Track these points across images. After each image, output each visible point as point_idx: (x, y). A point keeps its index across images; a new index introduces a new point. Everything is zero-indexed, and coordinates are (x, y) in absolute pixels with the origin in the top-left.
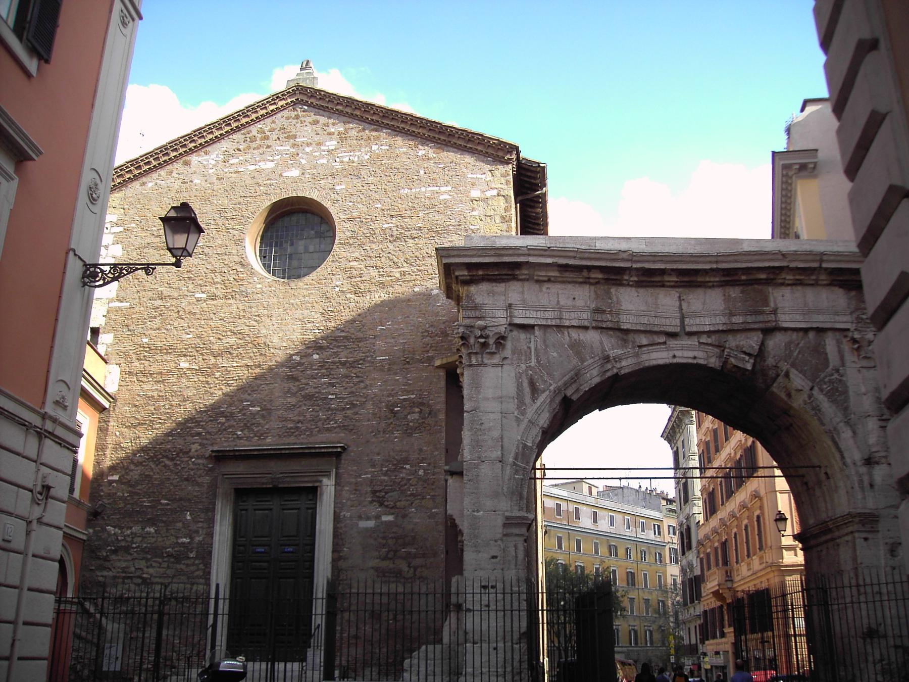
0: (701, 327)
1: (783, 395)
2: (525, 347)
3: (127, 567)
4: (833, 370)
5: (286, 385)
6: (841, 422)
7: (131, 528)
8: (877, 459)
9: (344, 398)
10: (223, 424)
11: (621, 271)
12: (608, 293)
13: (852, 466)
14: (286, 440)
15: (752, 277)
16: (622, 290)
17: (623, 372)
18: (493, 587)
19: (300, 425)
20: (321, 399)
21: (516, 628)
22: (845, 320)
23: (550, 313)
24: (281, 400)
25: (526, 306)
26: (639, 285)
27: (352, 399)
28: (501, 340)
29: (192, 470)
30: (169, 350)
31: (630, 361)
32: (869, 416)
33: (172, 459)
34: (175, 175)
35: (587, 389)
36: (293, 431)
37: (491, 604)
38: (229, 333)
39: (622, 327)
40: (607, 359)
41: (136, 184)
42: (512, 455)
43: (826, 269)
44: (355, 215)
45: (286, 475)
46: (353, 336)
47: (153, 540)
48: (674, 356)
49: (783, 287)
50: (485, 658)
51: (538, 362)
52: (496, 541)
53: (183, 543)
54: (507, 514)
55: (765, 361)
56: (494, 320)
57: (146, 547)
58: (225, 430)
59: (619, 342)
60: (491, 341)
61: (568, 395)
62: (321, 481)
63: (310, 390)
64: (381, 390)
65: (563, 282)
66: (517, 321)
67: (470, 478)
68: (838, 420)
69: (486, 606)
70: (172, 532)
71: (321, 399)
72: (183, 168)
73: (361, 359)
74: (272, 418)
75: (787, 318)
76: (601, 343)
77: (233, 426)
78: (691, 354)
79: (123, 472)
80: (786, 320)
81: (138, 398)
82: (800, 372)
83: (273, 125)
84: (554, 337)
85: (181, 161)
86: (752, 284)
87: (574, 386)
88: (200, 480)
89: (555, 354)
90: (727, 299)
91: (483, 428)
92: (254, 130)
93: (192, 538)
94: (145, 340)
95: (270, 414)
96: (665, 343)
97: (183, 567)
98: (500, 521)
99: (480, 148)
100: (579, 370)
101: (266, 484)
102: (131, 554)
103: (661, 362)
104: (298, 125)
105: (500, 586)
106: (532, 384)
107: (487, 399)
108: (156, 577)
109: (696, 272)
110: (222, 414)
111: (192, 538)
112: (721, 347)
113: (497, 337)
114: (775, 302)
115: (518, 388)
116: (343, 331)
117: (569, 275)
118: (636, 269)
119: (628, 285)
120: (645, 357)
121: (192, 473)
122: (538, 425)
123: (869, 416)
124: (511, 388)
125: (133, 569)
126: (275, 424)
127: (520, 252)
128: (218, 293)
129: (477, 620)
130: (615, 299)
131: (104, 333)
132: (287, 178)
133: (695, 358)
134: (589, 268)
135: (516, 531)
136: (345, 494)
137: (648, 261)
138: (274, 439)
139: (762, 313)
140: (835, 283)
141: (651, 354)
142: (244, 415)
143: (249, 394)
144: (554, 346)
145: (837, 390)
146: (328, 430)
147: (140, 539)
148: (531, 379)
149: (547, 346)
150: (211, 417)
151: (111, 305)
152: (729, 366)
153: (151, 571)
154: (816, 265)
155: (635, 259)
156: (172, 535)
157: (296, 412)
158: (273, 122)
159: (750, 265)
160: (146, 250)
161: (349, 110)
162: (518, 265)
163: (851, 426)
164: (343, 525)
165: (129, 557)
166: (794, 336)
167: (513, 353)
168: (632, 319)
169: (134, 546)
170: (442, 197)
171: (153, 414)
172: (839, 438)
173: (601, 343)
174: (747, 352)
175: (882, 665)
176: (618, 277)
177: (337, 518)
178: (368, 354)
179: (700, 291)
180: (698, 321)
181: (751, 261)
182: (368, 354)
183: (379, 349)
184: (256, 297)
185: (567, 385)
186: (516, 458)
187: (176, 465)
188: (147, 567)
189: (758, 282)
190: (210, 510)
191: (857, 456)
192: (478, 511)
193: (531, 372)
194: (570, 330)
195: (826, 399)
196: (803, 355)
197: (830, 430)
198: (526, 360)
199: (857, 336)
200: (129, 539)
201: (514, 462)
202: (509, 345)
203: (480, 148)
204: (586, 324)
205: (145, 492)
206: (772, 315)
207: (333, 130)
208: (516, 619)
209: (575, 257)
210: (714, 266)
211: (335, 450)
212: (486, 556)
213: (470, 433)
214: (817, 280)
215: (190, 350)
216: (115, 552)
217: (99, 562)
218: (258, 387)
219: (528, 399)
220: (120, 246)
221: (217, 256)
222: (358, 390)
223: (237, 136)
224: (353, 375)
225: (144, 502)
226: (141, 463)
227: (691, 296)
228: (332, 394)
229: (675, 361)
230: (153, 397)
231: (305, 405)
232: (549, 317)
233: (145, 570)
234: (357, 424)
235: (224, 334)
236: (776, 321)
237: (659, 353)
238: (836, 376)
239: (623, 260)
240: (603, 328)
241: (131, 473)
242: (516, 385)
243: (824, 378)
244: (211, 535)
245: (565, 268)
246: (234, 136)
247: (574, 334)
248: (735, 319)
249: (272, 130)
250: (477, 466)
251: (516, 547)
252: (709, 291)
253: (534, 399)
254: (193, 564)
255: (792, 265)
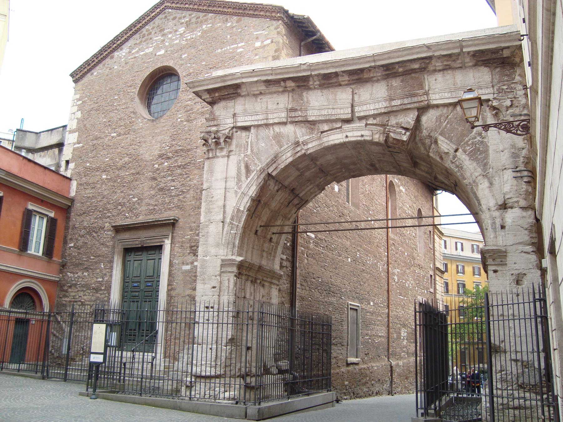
0: (368, 112)
1: (438, 159)
2: (245, 142)
3: (75, 296)
4: (476, 134)
5: (151, 183)
6: (480, 175)
7: (77, 273)
8: (510, 205)
9: (178, 188)
10: (120, 210)
11: (305, 79)
12: (301, 96)
13: (487, 211)
14: (149, 217)
15: (407, 68)
16: (311, 93)
17: (309, 152)
18: (212, 308)
19: (156, 207)
20: (167, 190)
21: (224, 336)
22: (487, 92)
23: (260, 116)
24: (148, 193)
25: (246, 113)
26: (322, 86)
27: (183, 188)
28: (228, 138)
29: (105, 238)
30: (98, 169)
31: (314, 144)
32: (505, 169)
33: (96, 233)
34: (106, 65)
35: (283, 167)
36: (152, 211)
37: (210, 319)
38: (125, 155)
39: (309, 120)
40: (297, 144)
41: (89, 75)
42: (230, 217)
43: (468, 53)
44: (191, 71)
45: (147, 239)
46: (185, 149)
47: (86, 280)
48: (347, 136)
49: (436, 73)
50: (204, 355)
51: (252, 151)
52: (216, 276)
53: (99, 281)
54: (223, 258)
55: (422, 133)
56: (225, 126)
57: (84, 284)
58: (121, 213)
59: (308, 131)
60: (222, 140)
61: (270, 172)
62: (164, 242)
63: (162, 185)
64: (198, 181)
65: (271, 93)
66: (239, 124)
67: (203, 234)
68: (477, 174)
69: (207, 320)
70: (95, 275)
71: (167, 190)
72: (110, 60)
73: (189, 163)
74: (143, 204)
75: (437, 97)
76: (295, 133)
77: (125, 211)
78: (359, 133)
79: (76, 241)
80: (436, 98)
81: (84, 198)
82: (447, 139)
83: (154, 25)
84: (263, 132)
85: (109, 57)
86: (410, 74)
87: (274, 166)
88: (108, 244)
89: (263, 145)
90: (390, 88)
91: (213, 199)
92: (144, 30)
93: (103, 278)
94: (88, 164)
95: (142, 202)
96: (341, 127)
97: (99, 295)
98: (219, 263)
99: (262, 13)
100: (277, 154)
101: (138, 244)
102: (77, 288)
103: (337, 142)
104: (166, 22)
105: (216, 307)
106: (247, 167)
107: (217, 180)
108: (87, 301)
109: (362, 70)
110: (120, 204)
111: (103, 278)
112: (383, 125)
113: (225, 137)
114: (429, 85)
115: (238, 171)
116: (180, 146)
117: (274, 89)
118: (315, 75)
119: (315, 88)
120: (325, 139)
121: (105, 240)
122: (248, 195)
123: (505, 169)
124: (233, 171)
125: (77, 297)
126: (144, 208)
127: (236, 76)
128: (122, 132)
129: (201, 329)
130: (305, 99)
131: (71, 163)
132: (159, 55)
133: (362, 136)
134: (284, 80)
135: (229, 269)
136: (176, 249)
137: (322, 68)
138: (143, 217)
139: (415, 95)
140: (480, 63)
141: (330, 137)
142: (130, 203)
143: (133, 191)
144: (263, 139)
145: (479, 150)
146: (170, 209)
147: (81, 279)
148: (247, 163)
149: (258, 140)
150: (115, 206)
151: (74, 146)
152: (391, 140)
153: (85, 297)
154: (457, 51)
155: (312, 68)
156: (95, 277)
157: (154, 199)
158: (154, 23)
159: (401, 59)
160: (91, 112)
161: (191, 6)
162: (237, 86)
163: (489, 179)
164: (174, 268)
165: (76, 290)
166: (445, 110)
167: (237, 146)
168: (316, 113)
169: (79, 283)
170: (239, 51)
171: (89, 207)
172: (477, 190)
173: (295, 133)
174: (405, 127)
175: (501, 375)
176: (305, 84)
177: (171, 264)
178: (192, 159)
179: (369, 86)
180: (365, 108)
181: (402, 56)
182: (192, 159)
183: (198, 155)
184: (139, 131)
185: (269, 165)
186: (232, 219)
187: (98, 236)
188: (84, 295)
189: (413, 71)
190: (111, 262)
191: (492, 203)
192: (206, 256)
193: (246, 159)
194: (274, 126)
195: (467, 158)
196: (451, 125)
197: (470, 183)
198: (244, 151)
199: (495, 103)
200: (76, 280)
201: (231, 222)
202: (234, 142)
203: (262, 13)
204: (284, 120)
205: (84, 252)
206: (425, 96)
207: (183, 21)
208: (225, 329)
209: (272, 74)
210: (373, 64)
211: (170, 222)
212: (209, 286)
213: (205, 204)
214: (463, 63)
215: (107, 168)
216: (70, 287)
217: (64, 293)
218: (137, 186)
219: (243, 178)
220: (80, 112)
221: (122, 110)
222: (186, 183)
223: (137, 36)
224: (184, 173)
225: (84, 258)
226: (83, 236)
227: (362, 90)
228: (173, 187)
229: (347, 140)
230: (90, 197)
231: (159, 194)
232: (259, 119)
233: (83, 296)
234: (185, 204)
235: (123, 156)
236: (428, 100)
237: (336, 135)
238: (478, 138)
239: (305, 70)
240: (296, 122)
241: (79, 242)
242: (237, 168)
243: (468, 141)
244: (111, 276)
245: (268, 82)
246: (135, 37)
247: (277, 129)
248: (394, 103)
249: (153, 29)
250: (207, 226)
251: (228, 280)
252: (376, 84)
253: (247, 177)
254: (104, 294)
255: (436, 54)
